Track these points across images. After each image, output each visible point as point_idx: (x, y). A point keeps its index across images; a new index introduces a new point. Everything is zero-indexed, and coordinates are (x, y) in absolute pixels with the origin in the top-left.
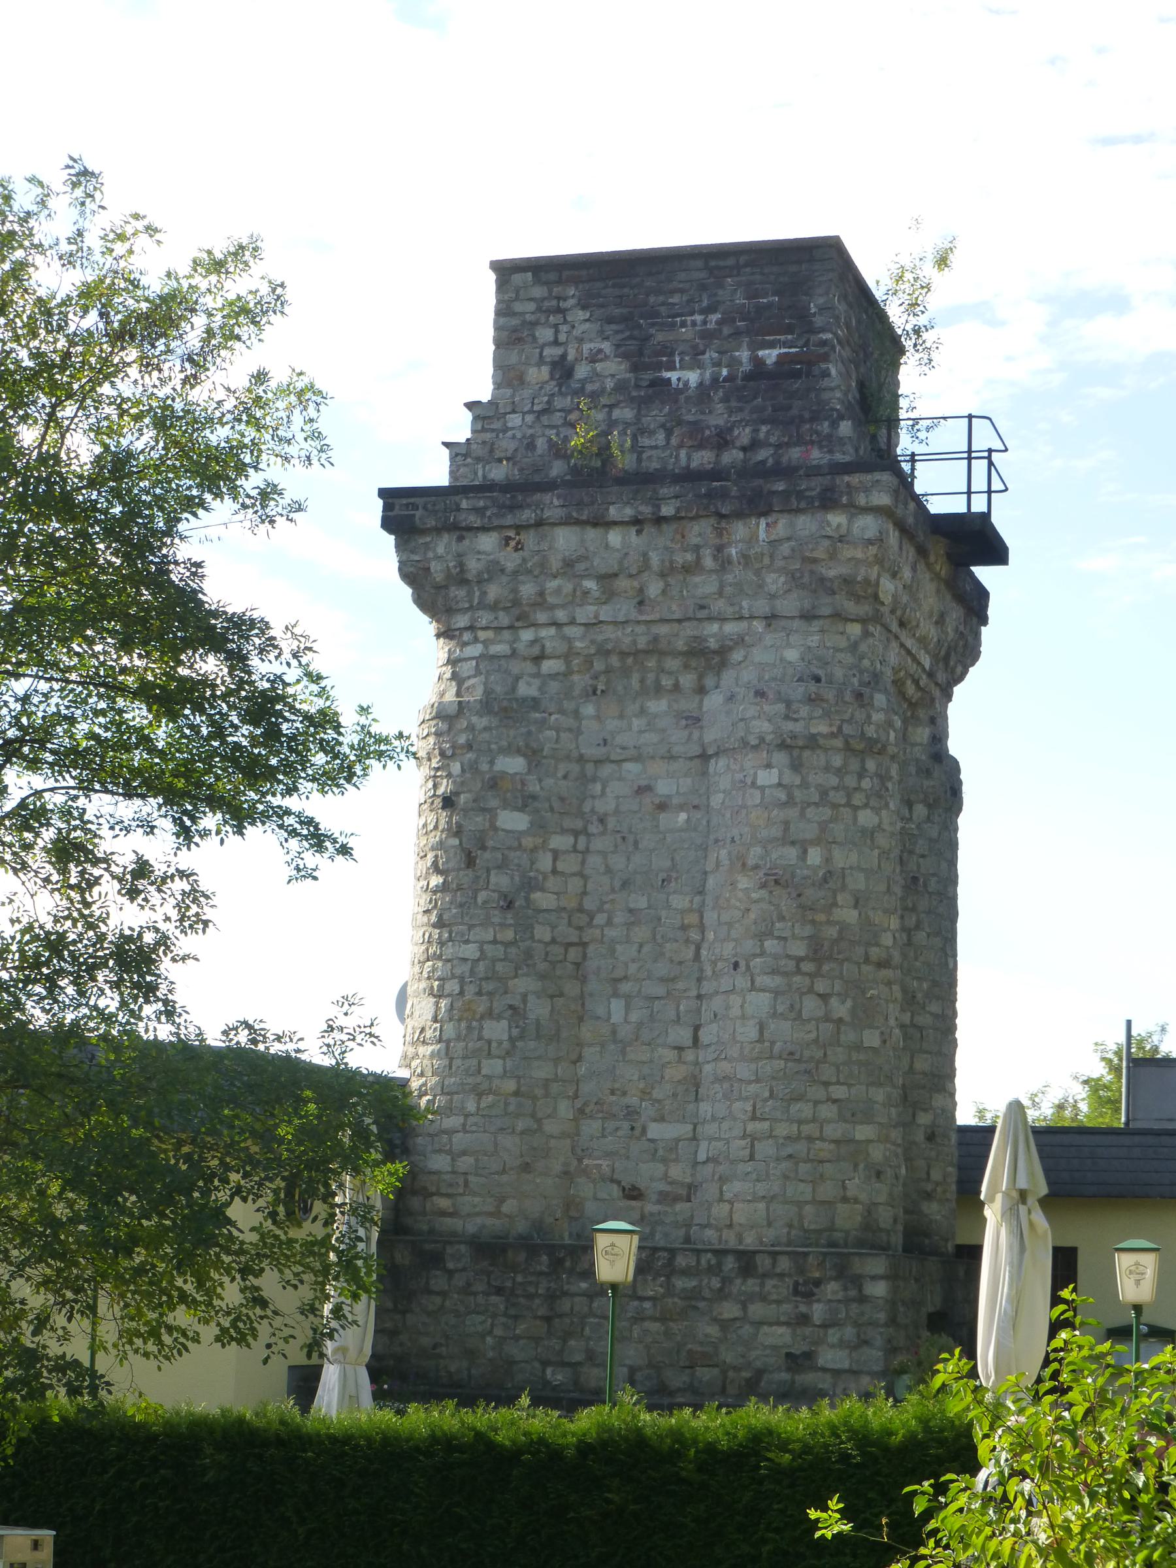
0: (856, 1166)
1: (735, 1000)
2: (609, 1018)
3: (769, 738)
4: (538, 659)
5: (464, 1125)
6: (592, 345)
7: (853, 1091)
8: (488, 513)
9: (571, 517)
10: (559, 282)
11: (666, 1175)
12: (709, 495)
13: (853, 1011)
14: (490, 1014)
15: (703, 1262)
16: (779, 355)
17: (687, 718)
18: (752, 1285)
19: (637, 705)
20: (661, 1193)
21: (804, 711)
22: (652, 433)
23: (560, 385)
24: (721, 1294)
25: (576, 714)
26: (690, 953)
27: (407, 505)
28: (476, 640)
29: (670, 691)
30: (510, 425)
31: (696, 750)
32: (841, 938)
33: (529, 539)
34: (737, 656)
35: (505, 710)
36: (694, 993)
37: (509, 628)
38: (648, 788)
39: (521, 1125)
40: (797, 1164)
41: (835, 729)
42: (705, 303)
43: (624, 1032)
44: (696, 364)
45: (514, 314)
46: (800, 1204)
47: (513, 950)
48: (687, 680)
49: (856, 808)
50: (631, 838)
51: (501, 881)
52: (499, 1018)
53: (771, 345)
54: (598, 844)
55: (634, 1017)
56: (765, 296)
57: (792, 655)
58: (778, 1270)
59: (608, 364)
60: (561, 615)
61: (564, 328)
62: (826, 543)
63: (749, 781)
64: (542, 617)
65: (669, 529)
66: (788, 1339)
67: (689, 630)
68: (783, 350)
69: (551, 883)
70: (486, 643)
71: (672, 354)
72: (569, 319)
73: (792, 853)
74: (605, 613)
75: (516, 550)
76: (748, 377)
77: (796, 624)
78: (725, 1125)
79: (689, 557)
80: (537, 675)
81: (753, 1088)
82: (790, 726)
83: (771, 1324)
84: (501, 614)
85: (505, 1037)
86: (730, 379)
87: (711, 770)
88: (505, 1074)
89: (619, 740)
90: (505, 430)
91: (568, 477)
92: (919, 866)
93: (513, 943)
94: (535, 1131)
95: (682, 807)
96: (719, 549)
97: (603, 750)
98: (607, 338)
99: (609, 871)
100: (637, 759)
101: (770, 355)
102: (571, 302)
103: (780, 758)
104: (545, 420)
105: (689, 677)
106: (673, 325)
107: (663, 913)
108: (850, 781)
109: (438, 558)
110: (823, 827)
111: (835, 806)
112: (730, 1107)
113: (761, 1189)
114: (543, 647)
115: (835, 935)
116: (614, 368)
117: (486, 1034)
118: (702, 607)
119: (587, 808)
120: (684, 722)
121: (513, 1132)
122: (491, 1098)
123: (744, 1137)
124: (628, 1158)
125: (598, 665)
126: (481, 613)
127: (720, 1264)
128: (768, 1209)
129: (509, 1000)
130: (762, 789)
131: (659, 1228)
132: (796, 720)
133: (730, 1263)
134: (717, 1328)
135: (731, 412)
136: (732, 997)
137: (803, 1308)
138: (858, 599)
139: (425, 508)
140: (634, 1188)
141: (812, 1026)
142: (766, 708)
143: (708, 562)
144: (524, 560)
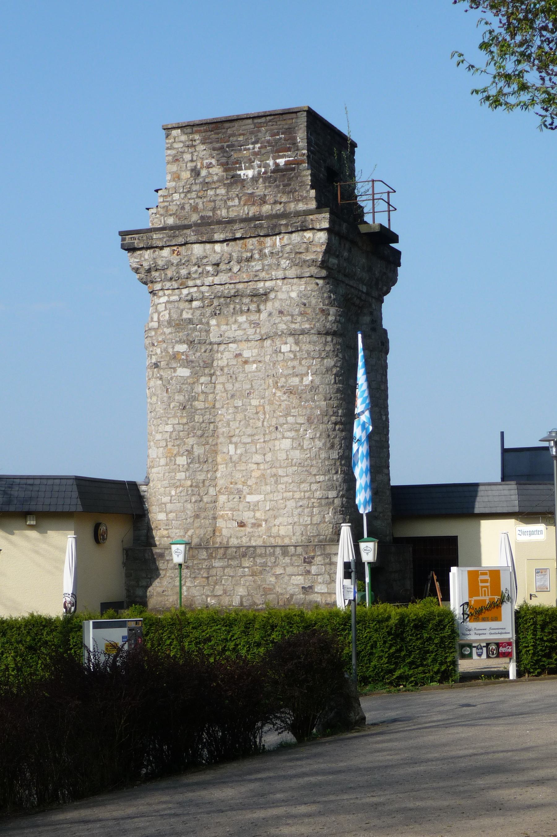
1: (277, 443)
2: (228, 453)
3: (285, 331)
4: (191, 301)
5: (171, 500)
6: (207, 161)
8: (165, 240)
9: (199, 240)
10: (192, 133)
11: (254, 516)
12: (255, 227)
14: (178, 454)
15: (268, 551)
16: (285, 162)
17: (254, 324)
18: (287, 560)
19: (234, 319)
20: (252, 524)
21: (299, 319)
22: (233, 199)
23: (195, 180)
24: (275, 564)
25: (208, 323)
26: (260, 424)
27: (131, 238)
28: (164, 295)
29: (247, 312)
30: (174, 199)
31: (258, 337)
33: (182, 249)
34: (272, 295)
35: (177, 325)
36: (262, 440)
37: (177, 289)
38: (240, 355)
39: (193, 499)
40: (304, 509)
42: (253, 140)
43: (235, 458)
44: (251, 167)
45: (174, 148)
46: (306, 526)
47: (186, 427)
48: (253, 307)
50: (234, 376)
51: (180, 398)
52: (182, 455)
53: (282, 157)
54: (221, 379)
55: (239, 452)
56: (278, 135)
57: (294, 295)
58: (297, 553)
59: (214, 169)
60: (198, 282)
61: (196, 154)
62: (305, 245)
63: (278, 350)
64: (190, 283)
65: (240, 242)
66: (302, 581)
67: (252, 285)
68: (288, 159)
69: (202, 398)
70: (169, 296)
71: (240, 163)
72: (197, 149)
73: (296, 380)
74: (217, 280)
75: (178, 255)
76: (274, 172)
77: (295, 280)
78: (275, 494)
79: (249, 255)
80: (191, 308)
81: (286, 479)
82: (293, 326)
83: (295, 575)
84: (174, 283)
85: (185, 463)
86: (265, 173)
87: (265, 345)
88: (185, 479)
89: (226, 335)
90: (173, 201)
91: (199, 221)
93: (187, 423)
95: (254, 362)
96: (261, 251)
97: (221, 339)
98: (213, 157)
99: (226, 391)
100: (234, 342)
101: (281, 162)
102: (198, 142)
103: (291, 340)
104: (189, 196)
105: (254, 306)
106: (240, 150)
107: (249, 407)
109: (145, 260)
112: (277, 487)
113: (290, 520)
114: (192, 296)
116: (217, 171)
117: (177, 462)
118: (256, 276)
119: (215, 364)
120: (253, 325)
121: (191, 502)
122: (181, 488)
123: (282, 499)
124: (239, 510)
125: (216, 303)
126: (166, 283)
127: (274, 551)
128: (293, 528)
129: (185, 447)
130: (284, 353)
131: (252, 538)
132: (296, 323)
133: (278, 551)
134: (274, 578)
135: (266, 188)
136: (276, 441)
137: (308, 568)
139: (139, 239)
140: (242, 522)
141: (308, 452)
142: (284, 318)
143: (257, 256)
144: (181, 260)
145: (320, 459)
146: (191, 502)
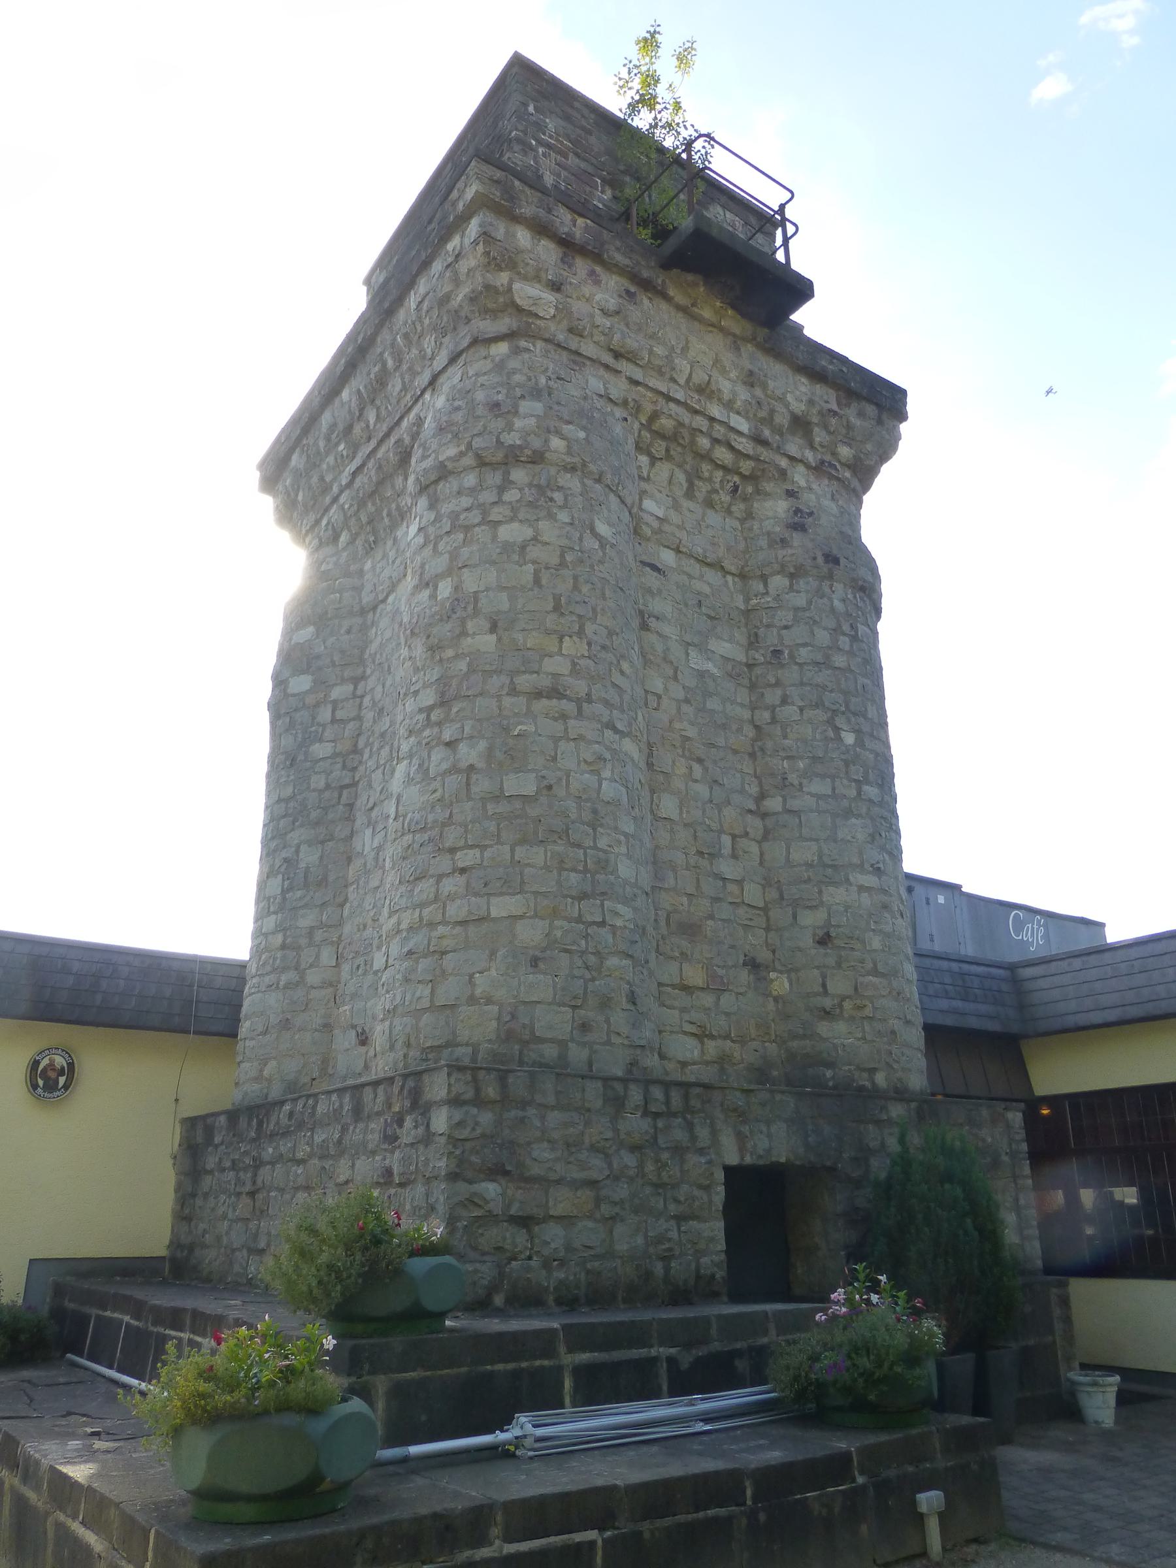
0: (493, 953)
7: (488, 854)
13: (489, 754)
32: (472, 670)
41: (463, 448)
49: (496, 524)
69: (328, 734)
92: (781, 638)
94: (297, 984)
108: (488, 497)
110: (454, 555)
111: (467, 529)
115: (465, 669)
121: (277, 987)
138: (494, 313)
145: (469, 798)
146: (277, 987)
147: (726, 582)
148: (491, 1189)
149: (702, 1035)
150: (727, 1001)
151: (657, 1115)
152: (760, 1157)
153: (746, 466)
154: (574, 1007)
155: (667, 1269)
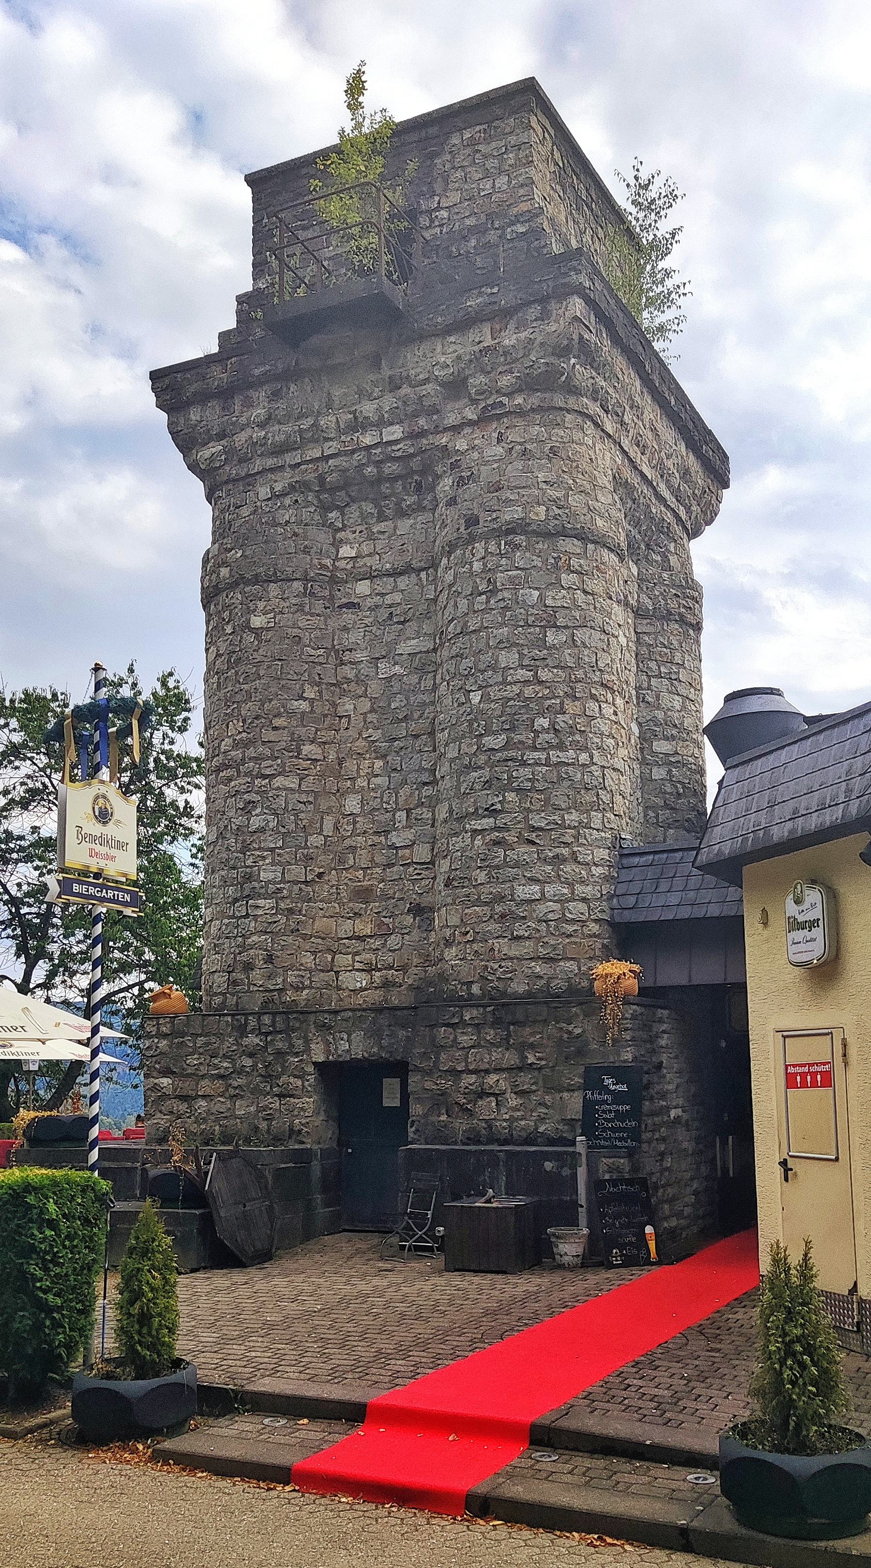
147: (420, 579)
148: (165, 1081)
149: (369, 969)
150: (393, 941)
151: (267, 1034)
152: (340, 1056)
153: (415, 463)
154: (229, 972)
155: (269, 1126)
